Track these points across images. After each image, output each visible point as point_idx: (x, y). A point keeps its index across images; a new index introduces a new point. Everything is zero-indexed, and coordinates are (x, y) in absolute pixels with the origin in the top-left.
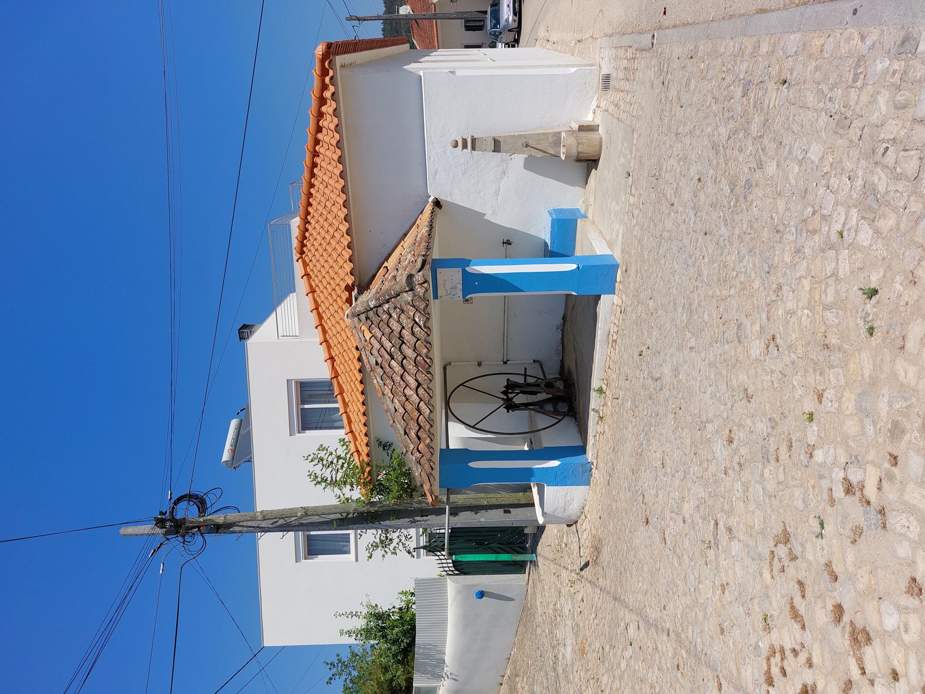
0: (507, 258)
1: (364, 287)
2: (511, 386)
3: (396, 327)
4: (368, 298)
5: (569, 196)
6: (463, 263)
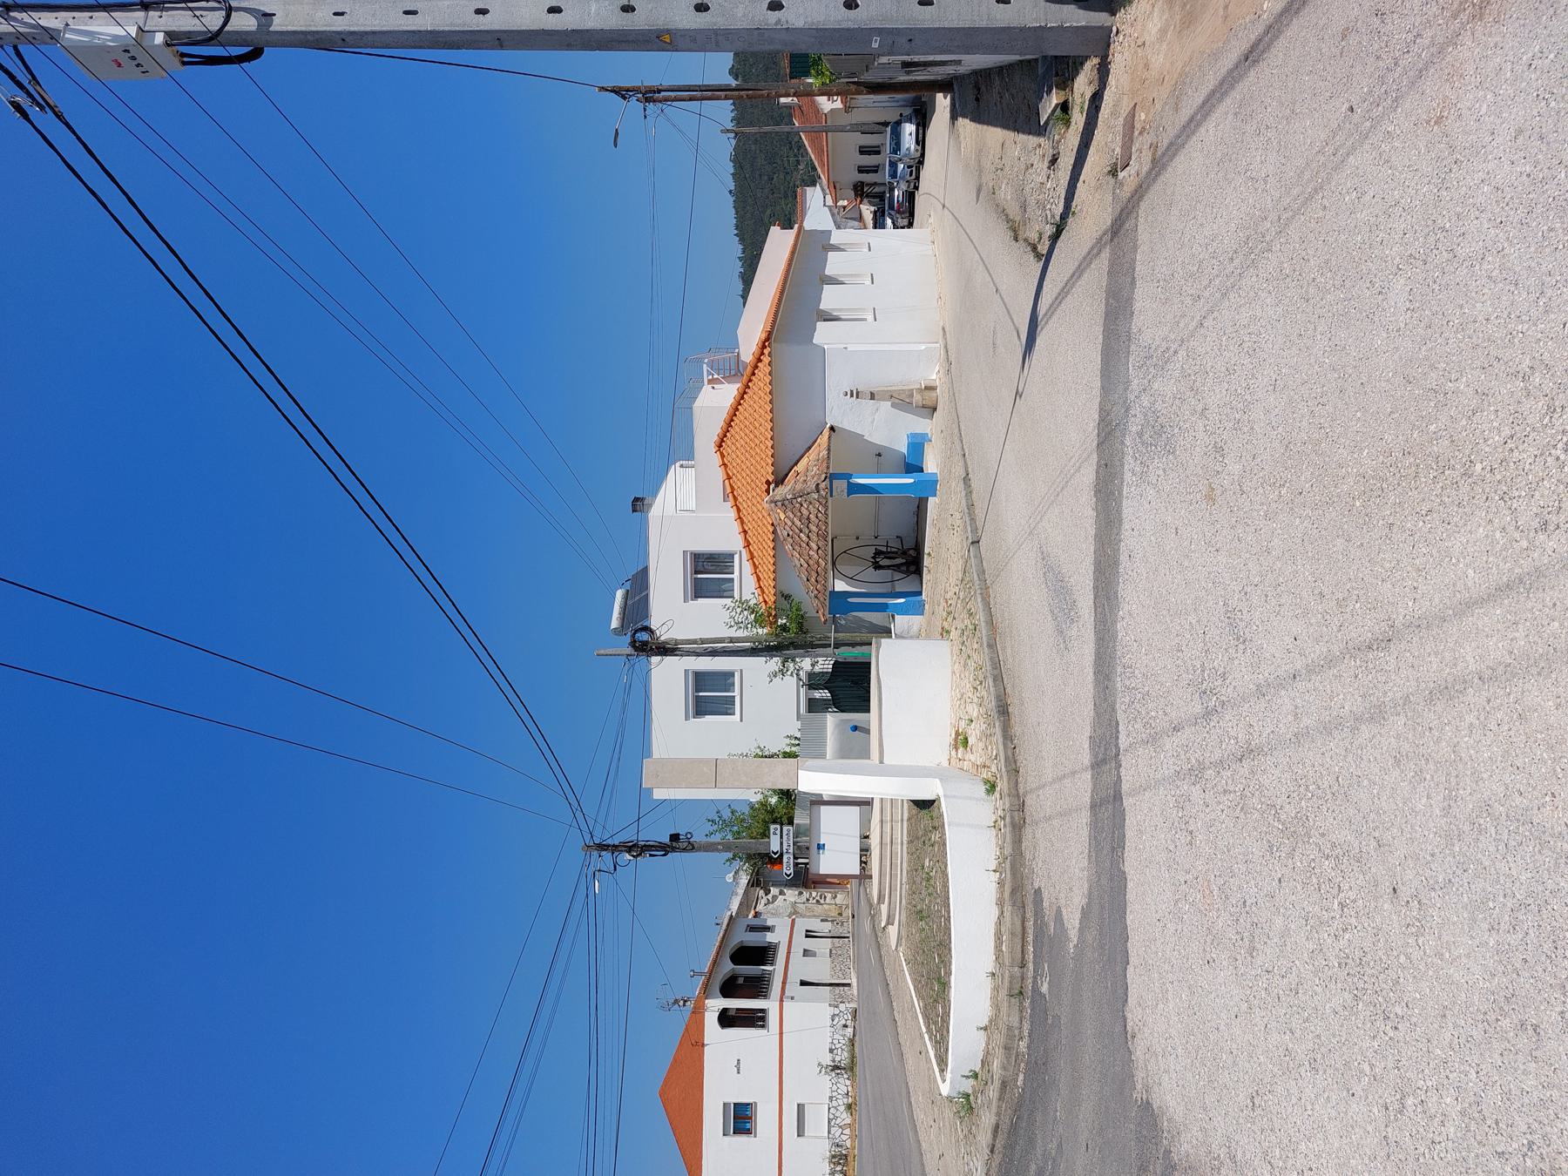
0: (879, 472)
1: (780, 481)
2: (878, 553)
3: (805, 512)
4: (782, 491)
5: (921, 425)
6: (848, 476)
